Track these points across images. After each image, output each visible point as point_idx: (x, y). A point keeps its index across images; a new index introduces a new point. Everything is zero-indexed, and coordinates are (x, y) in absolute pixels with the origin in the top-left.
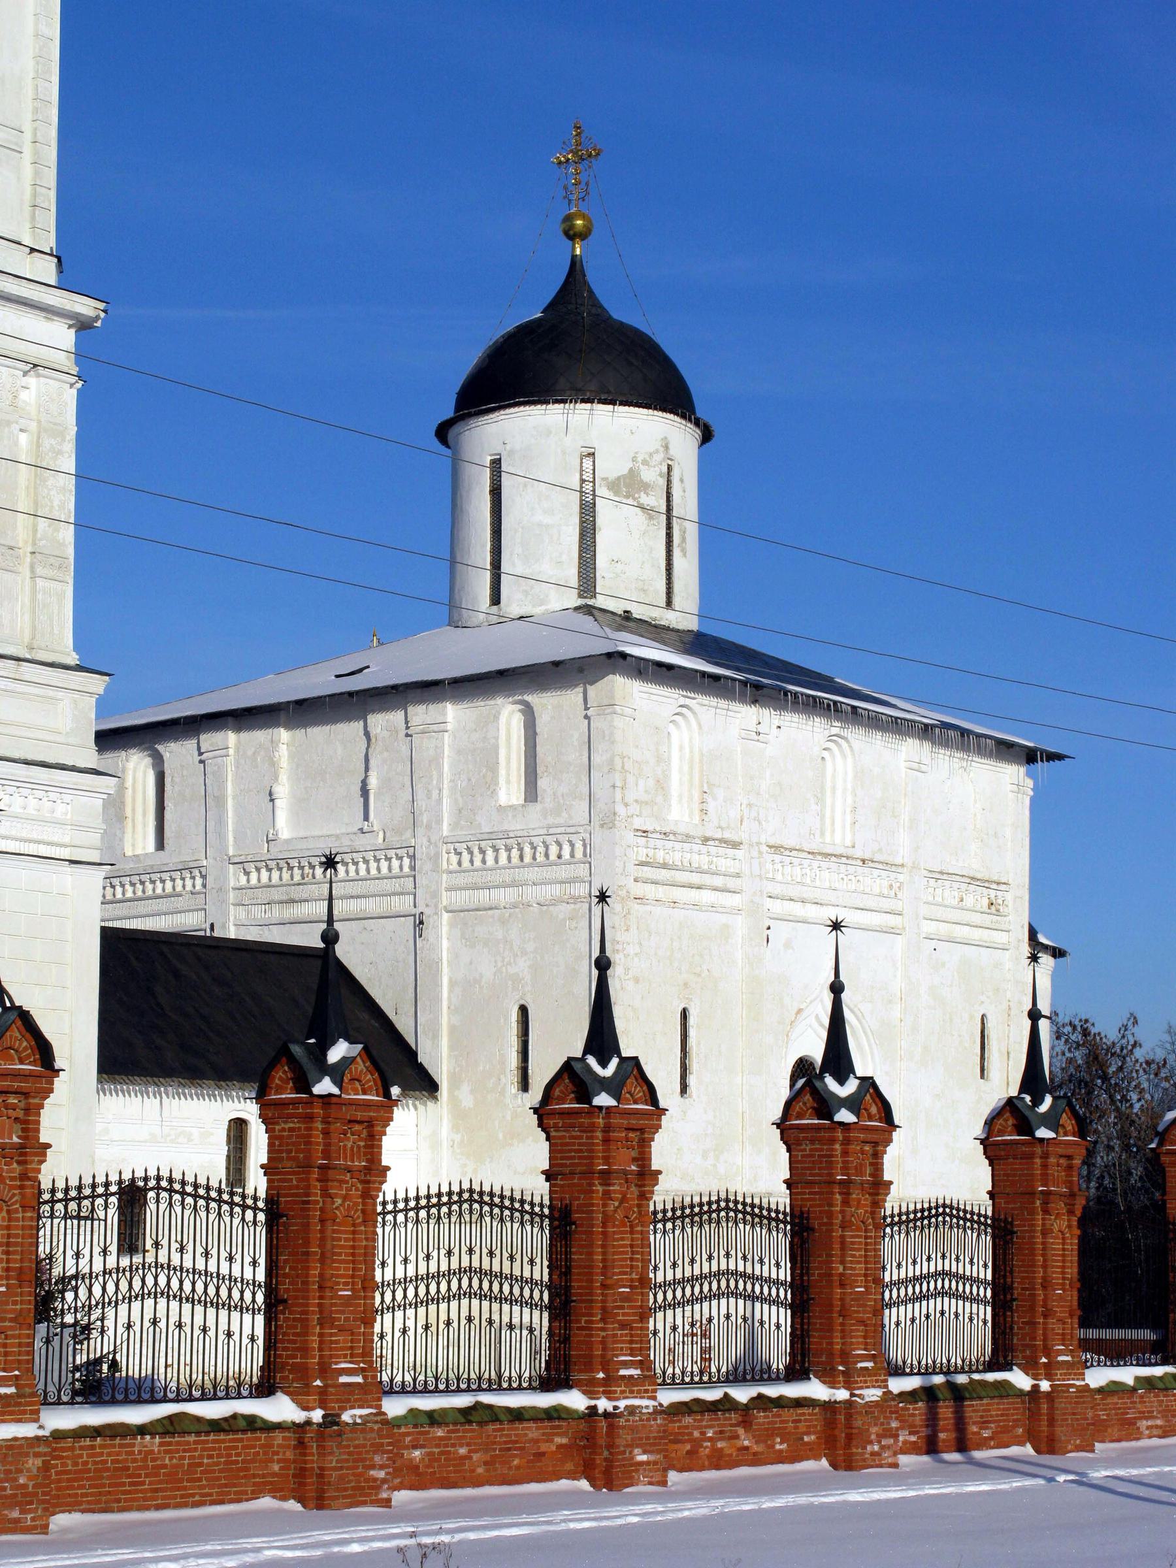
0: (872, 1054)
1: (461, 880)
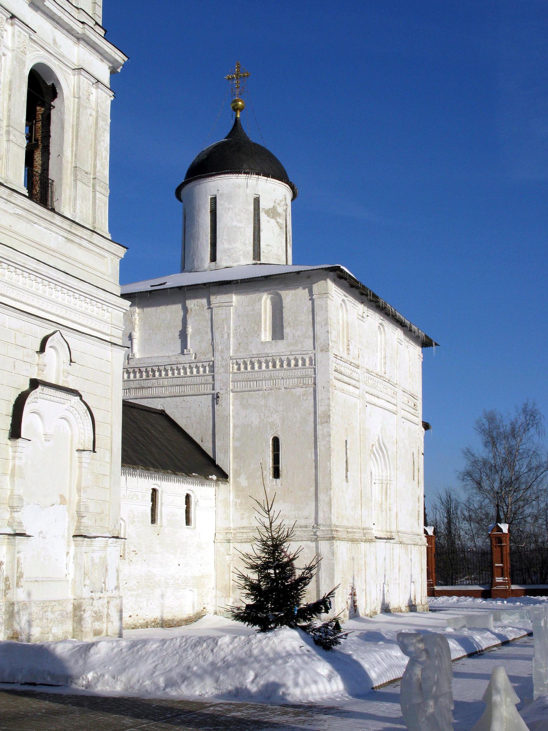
0: (390, 467)
1: (240, 377)
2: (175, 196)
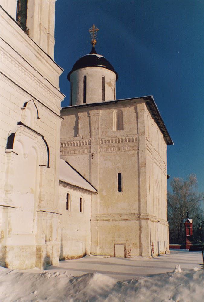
2: (67, 78)
